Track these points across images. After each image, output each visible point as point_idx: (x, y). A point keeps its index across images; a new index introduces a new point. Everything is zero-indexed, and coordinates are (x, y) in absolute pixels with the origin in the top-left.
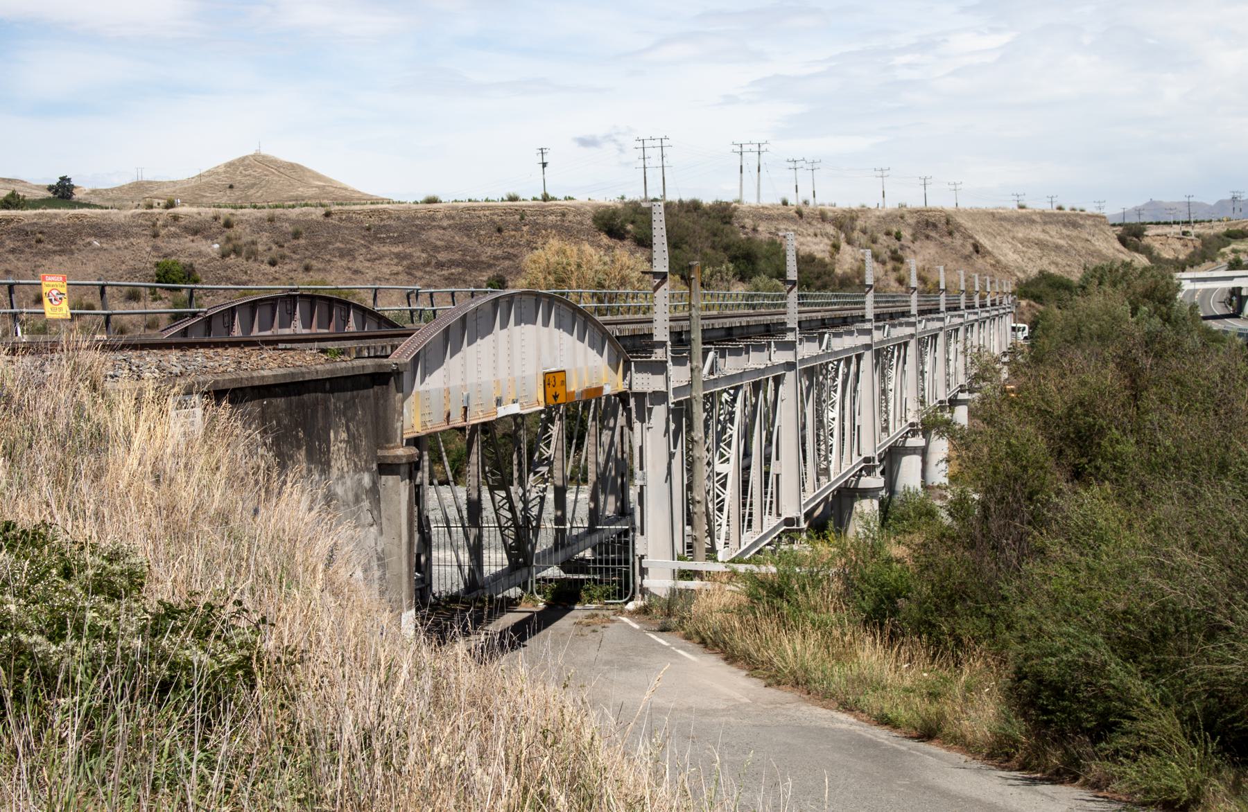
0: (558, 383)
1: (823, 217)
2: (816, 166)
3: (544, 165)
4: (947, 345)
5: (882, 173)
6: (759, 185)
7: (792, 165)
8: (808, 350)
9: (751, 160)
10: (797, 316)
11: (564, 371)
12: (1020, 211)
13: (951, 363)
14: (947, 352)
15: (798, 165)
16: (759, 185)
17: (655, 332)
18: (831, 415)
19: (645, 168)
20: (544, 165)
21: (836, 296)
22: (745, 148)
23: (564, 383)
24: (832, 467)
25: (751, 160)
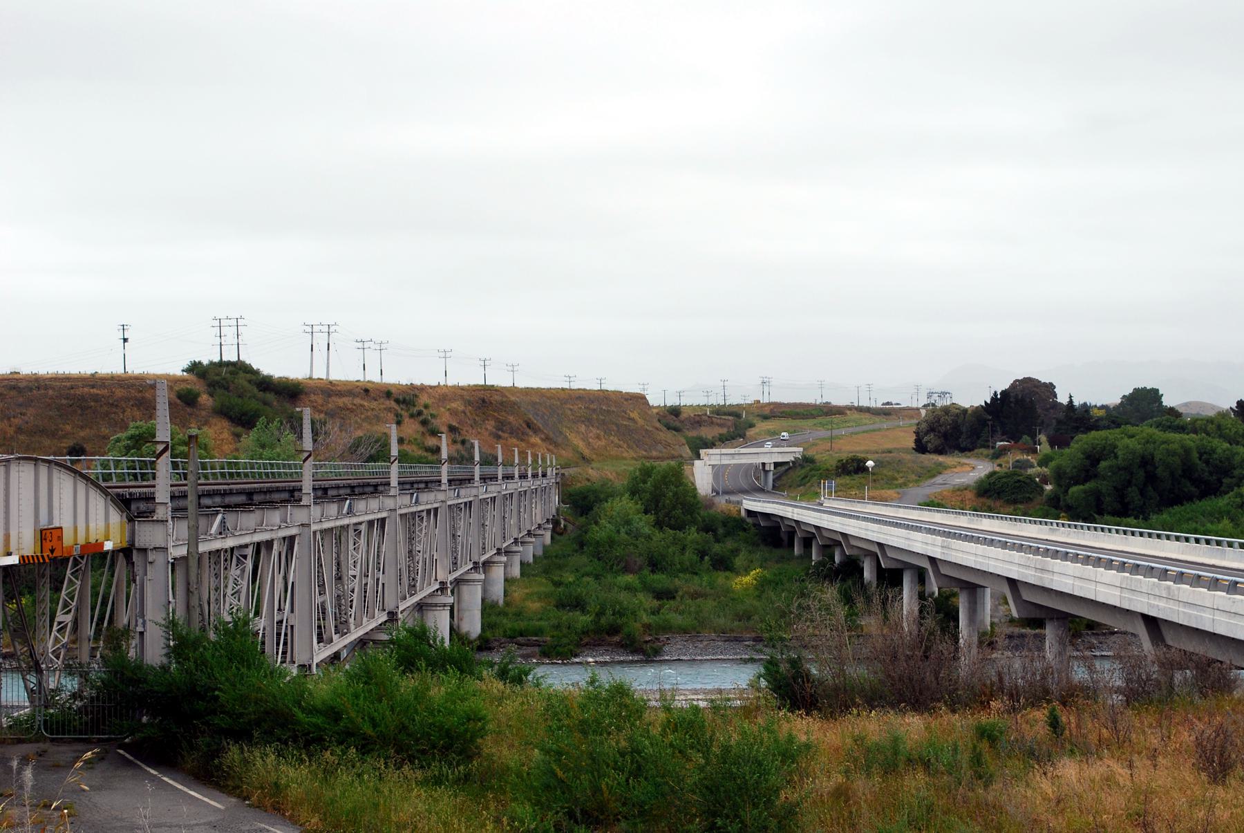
0: (55, 538)
1: (388, 394)
2: (383, 346)
3: (125, 340)
4: (520, 501)
5: (445, 355)
6: (328, 363)
7: (360, 345)
8: (330, 516)
9: (320, 341)
10: (170, 489)
11: (61, 528)
12: (566, 616)
13: (506, 520)
14: (520, 506)
15: (366, 345)
16: (328, 363)
17: (157, 495)
18: (418, 549)
19: (221, 345)
20: (125, 340)
21: (460, 468)
22: (316, 329)
23: (60, 538)
24: (418, 584)
25: (320, 341)
